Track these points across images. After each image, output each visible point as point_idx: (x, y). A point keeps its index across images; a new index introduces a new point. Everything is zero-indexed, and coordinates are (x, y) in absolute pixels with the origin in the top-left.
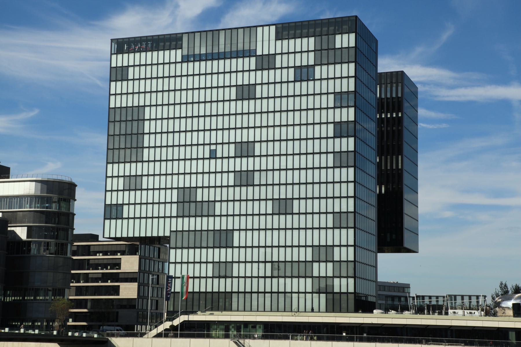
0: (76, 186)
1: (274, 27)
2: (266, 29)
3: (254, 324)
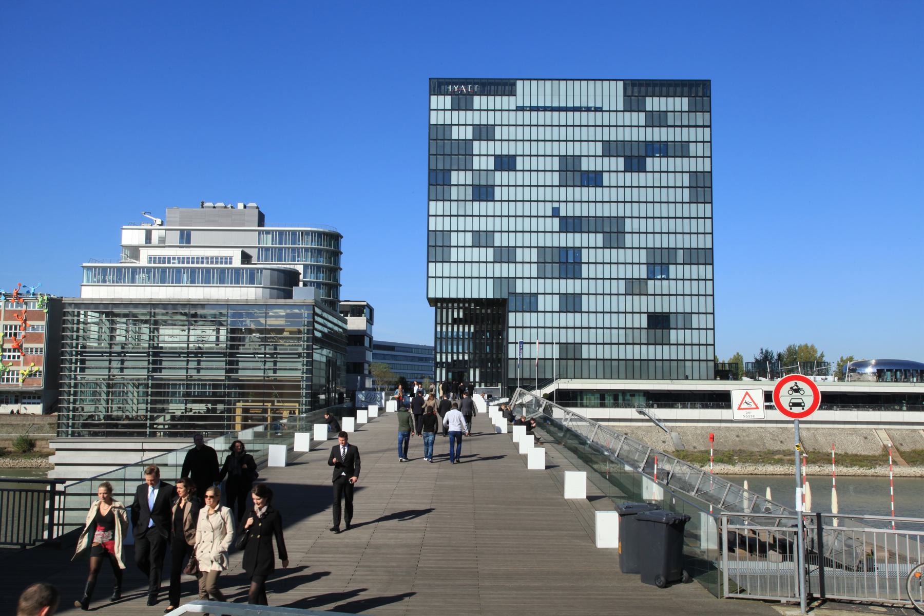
0: (342, 237)
1: (622, 82)
2: (613, 83)
3: (633, 393)
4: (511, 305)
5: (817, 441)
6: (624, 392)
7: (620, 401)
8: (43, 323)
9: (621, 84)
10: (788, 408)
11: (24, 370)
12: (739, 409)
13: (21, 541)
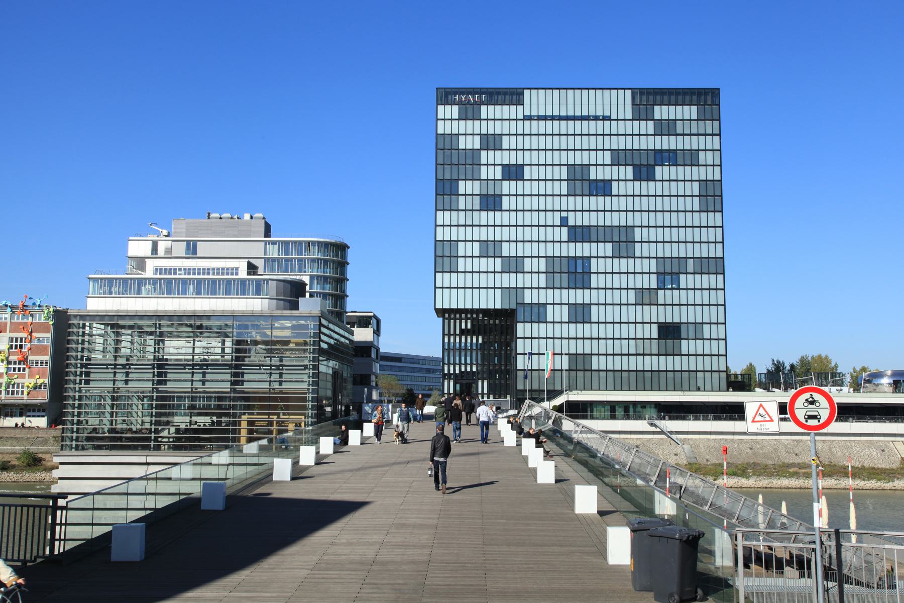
3: (644, 405)
4: (520, 316)
5: (832, 453)
6: (635, 404)
7: (631, 413)
8: (49, 335)
9: (629, 93)
10: (803, 421)
11: (29, 382)
12: (753, 421)
13: (22, 557)
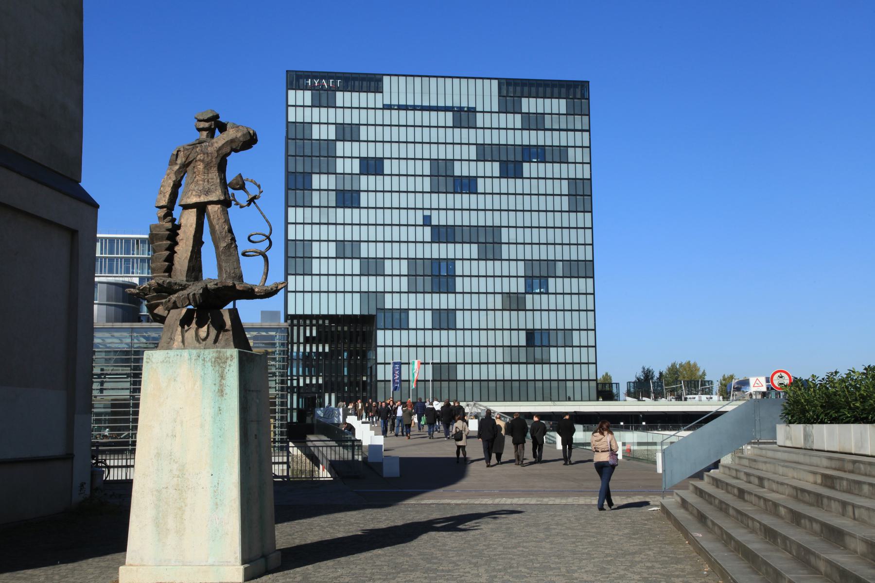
1: (496, 81)
9: (495, 83)
